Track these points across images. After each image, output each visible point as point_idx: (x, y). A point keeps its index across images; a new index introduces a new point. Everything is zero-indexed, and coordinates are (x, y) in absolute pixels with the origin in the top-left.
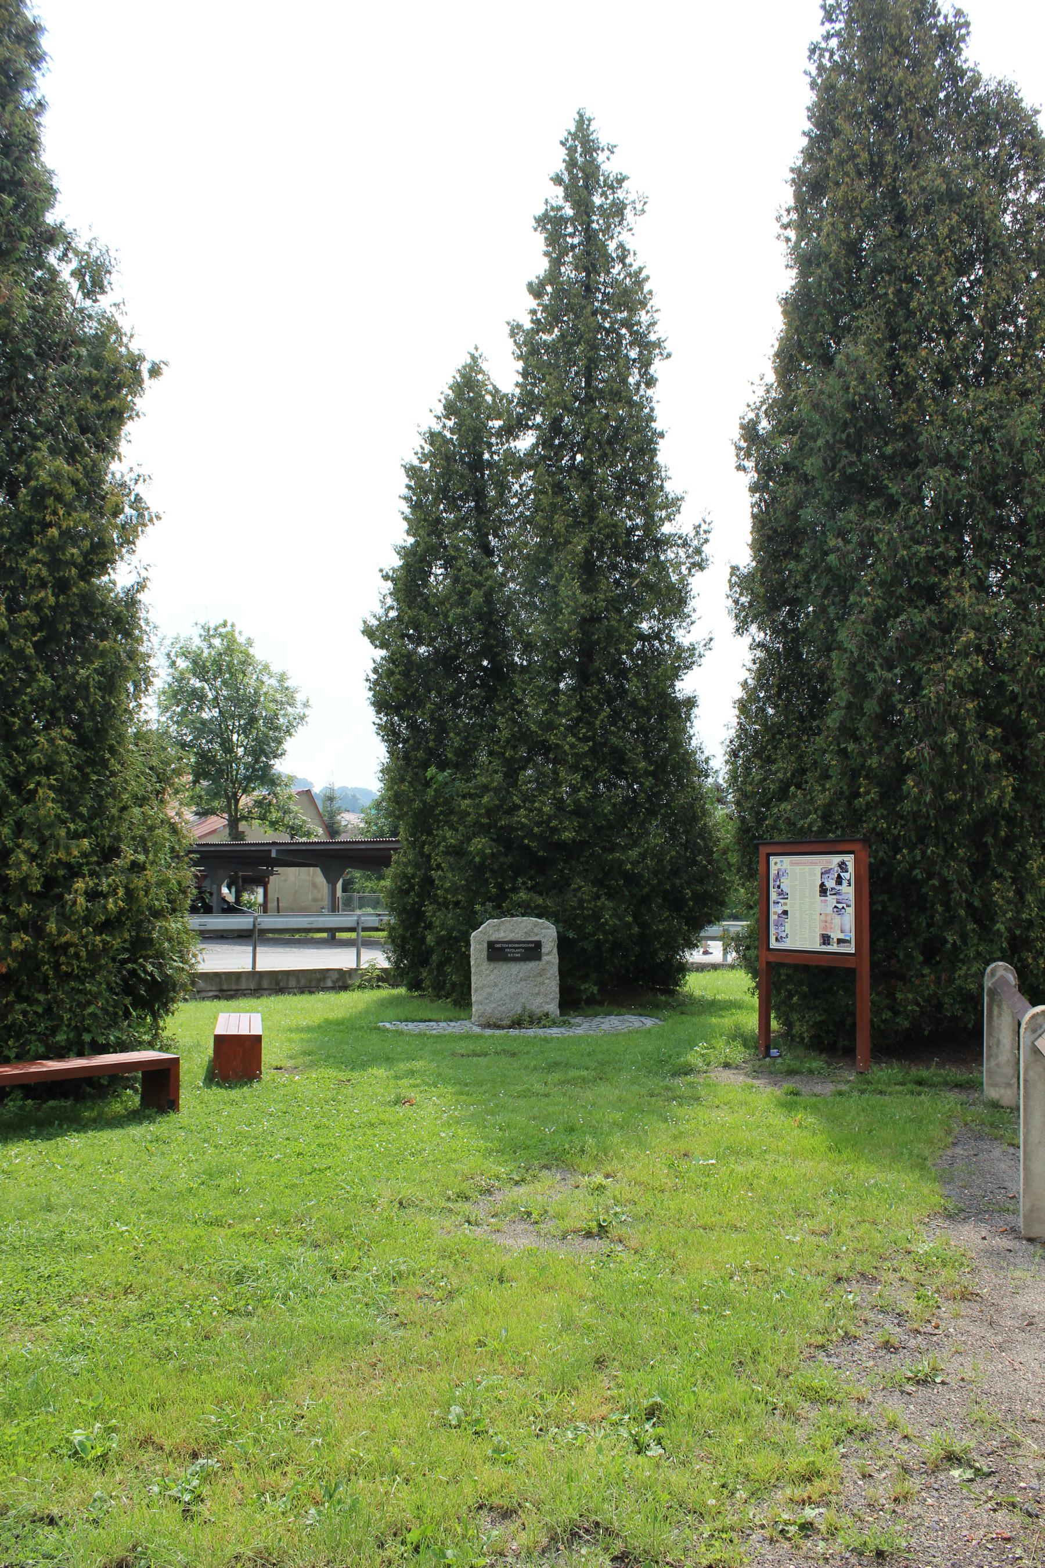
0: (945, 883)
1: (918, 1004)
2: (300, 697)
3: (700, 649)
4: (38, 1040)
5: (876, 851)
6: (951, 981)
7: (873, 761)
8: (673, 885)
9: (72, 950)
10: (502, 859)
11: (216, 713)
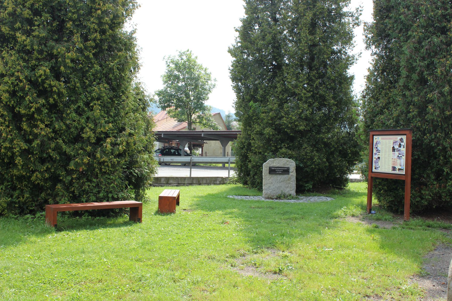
0: (444, 149)
1: (430, 196)
2: (212, 77)
3: (356, 57)
4: (94, 195)
5: (416, 135)
6: (445, 187)
7: (416, 99)
8: (343, 148)
9: (106, 164)
10: (277, 136)
11: (184, 83)
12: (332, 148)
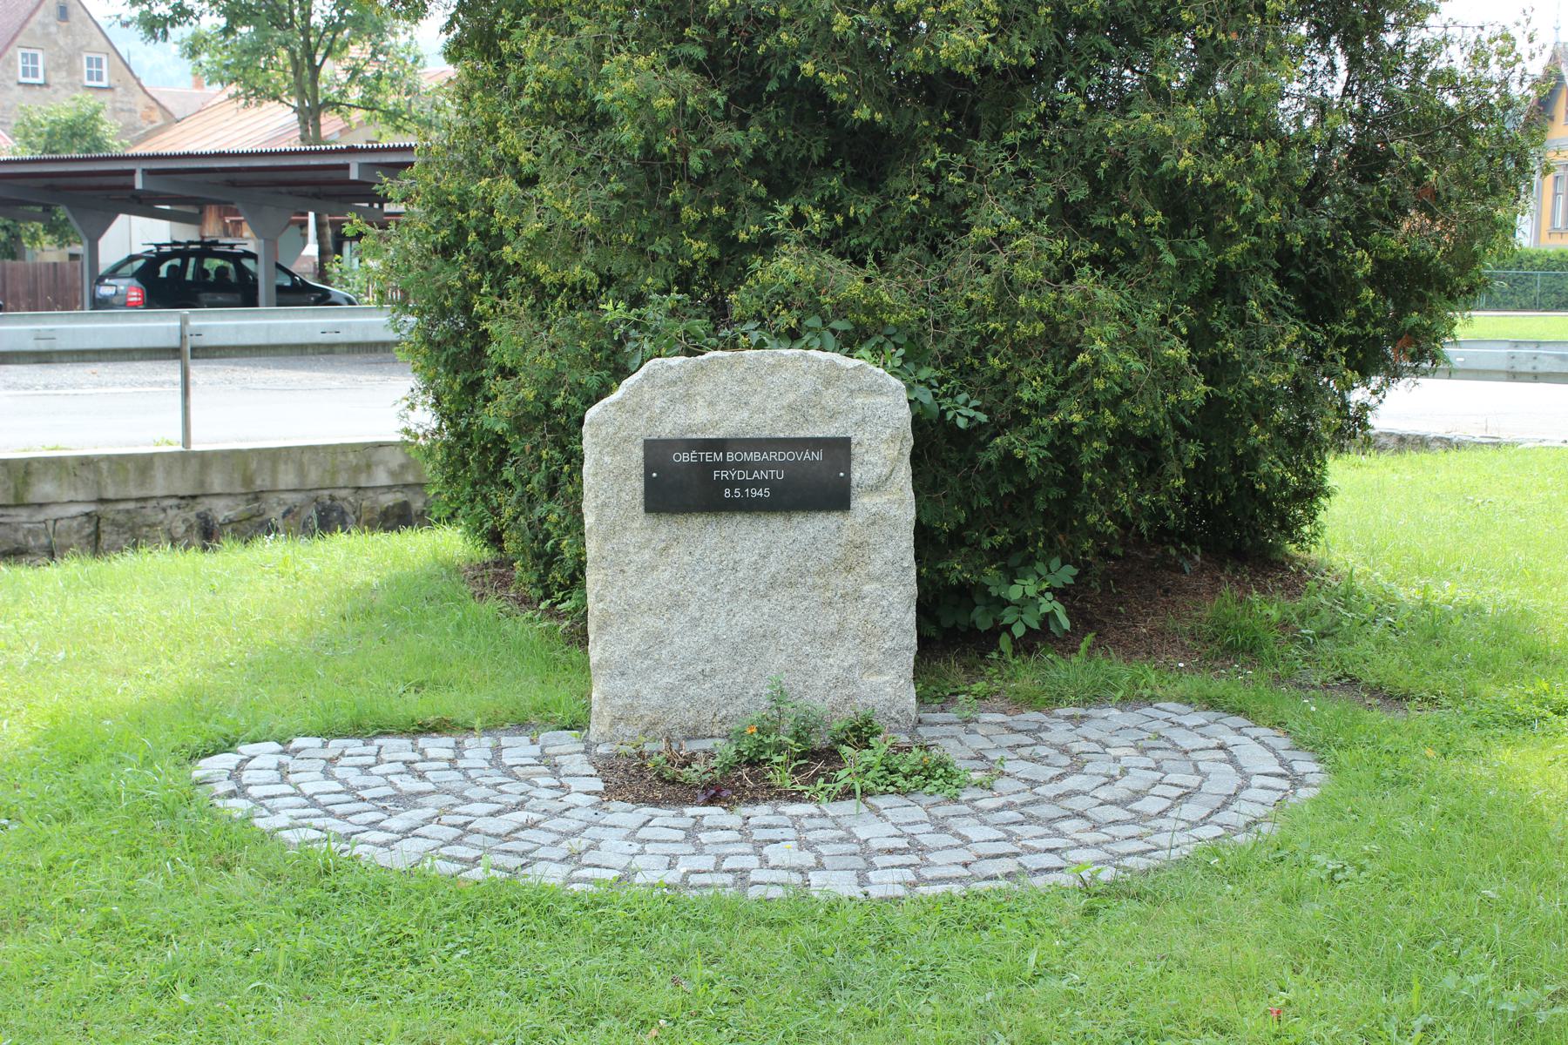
10: (726, 136)
12: (1233, 238)
